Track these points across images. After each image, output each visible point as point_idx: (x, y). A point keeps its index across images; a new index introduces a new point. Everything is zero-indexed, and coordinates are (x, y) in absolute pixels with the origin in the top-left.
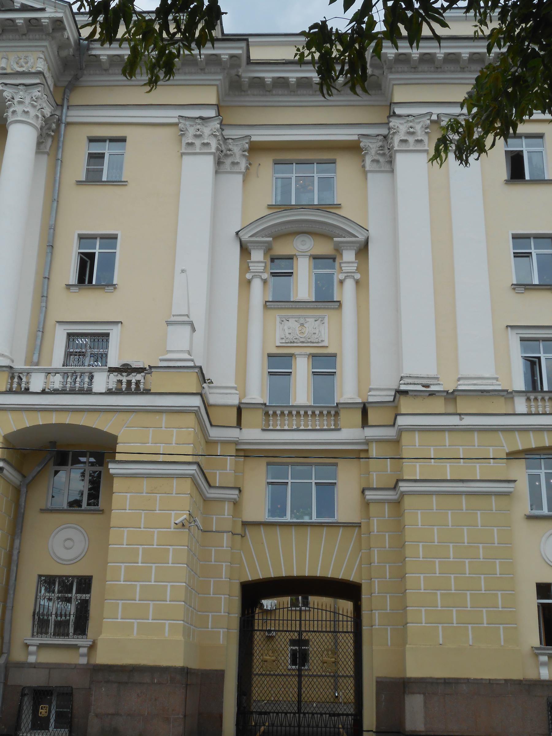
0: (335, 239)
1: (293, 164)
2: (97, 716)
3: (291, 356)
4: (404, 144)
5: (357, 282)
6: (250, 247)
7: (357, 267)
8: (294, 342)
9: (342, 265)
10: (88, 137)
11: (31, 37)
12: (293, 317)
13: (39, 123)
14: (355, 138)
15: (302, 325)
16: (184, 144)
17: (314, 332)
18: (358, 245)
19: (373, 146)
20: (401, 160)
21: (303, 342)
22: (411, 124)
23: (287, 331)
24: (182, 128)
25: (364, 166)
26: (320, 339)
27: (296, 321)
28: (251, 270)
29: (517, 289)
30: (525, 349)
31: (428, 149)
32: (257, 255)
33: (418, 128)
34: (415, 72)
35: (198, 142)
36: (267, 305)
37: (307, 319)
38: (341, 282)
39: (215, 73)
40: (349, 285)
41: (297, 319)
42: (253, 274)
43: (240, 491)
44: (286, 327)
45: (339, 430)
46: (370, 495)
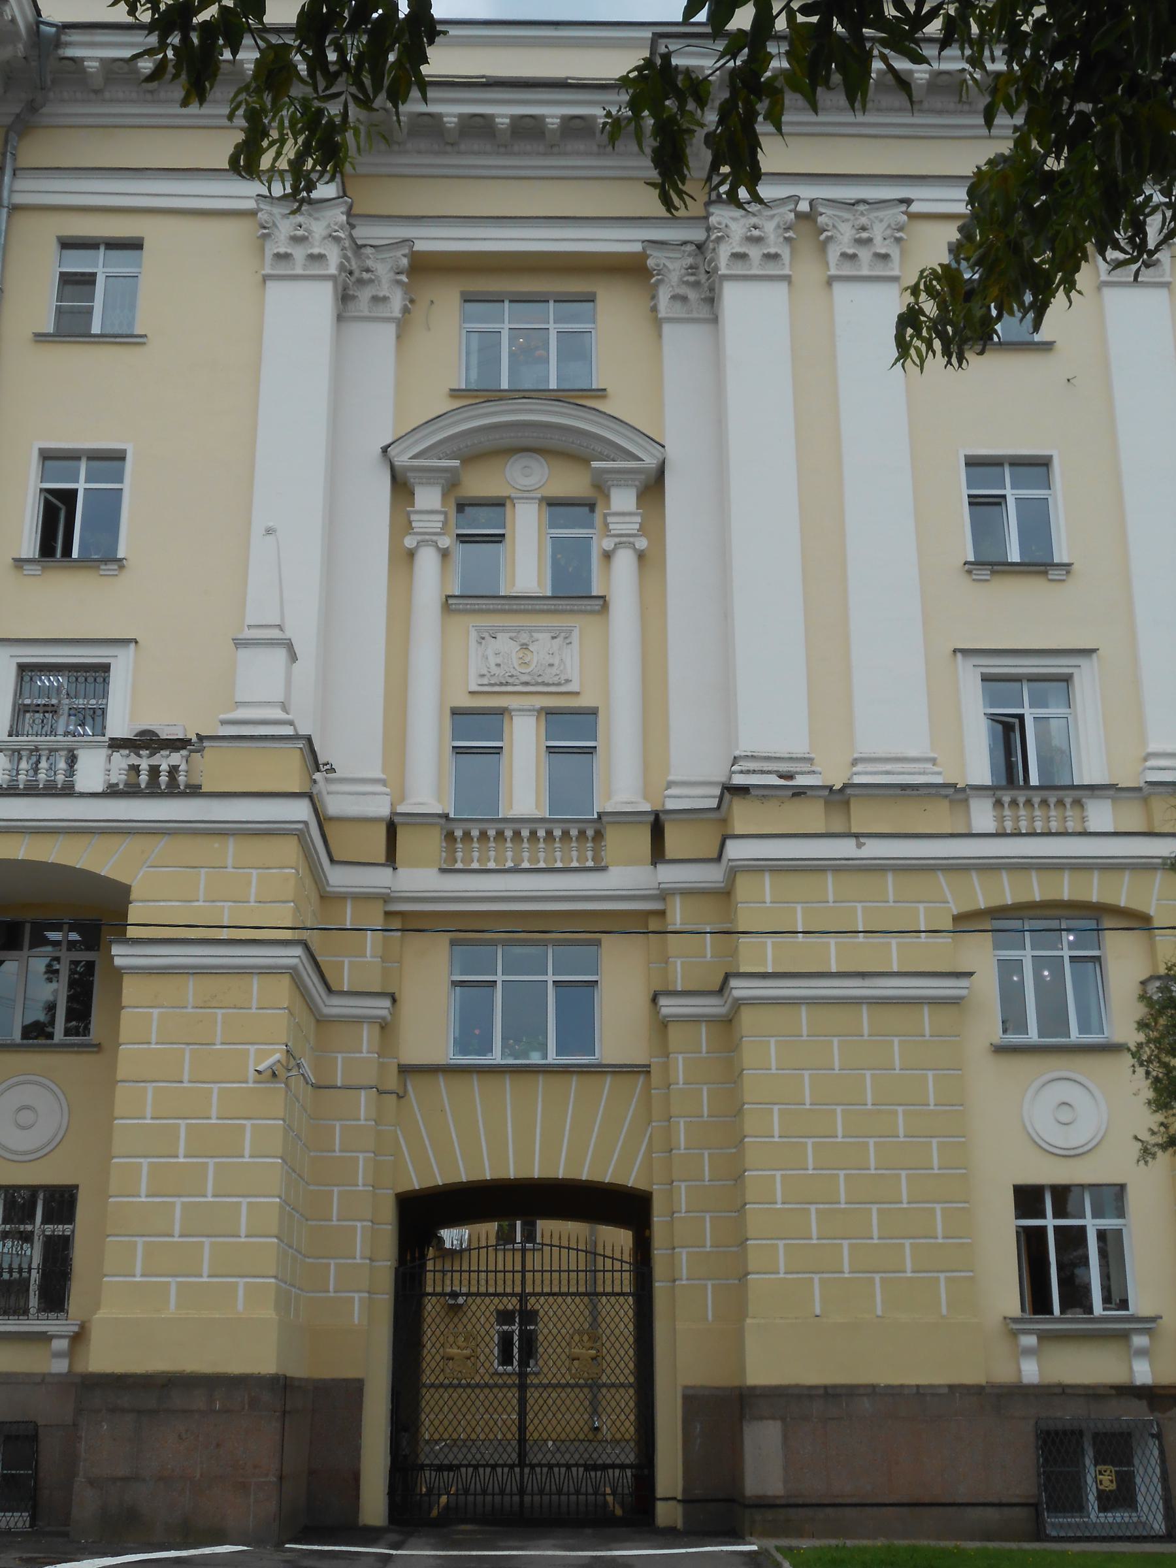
0: (595, 464)
1: (503, 301)
2: (92, 1482)
3: (502, 712)
5: (641, 556)
7: (641, 524)
8: (507, 684)
9: (610, 519)
12: (504, 630)
15: (525, 647)
16: (269, 254)
17: (551, 661)
18: (643, 477)
19: (674, 267)
20: (733, 296)
21: (526, 684)
23: (493, 661)
24: (266, 222)
25: (654, 309)
26: (563, 677)
27: (511, 638)
28: (415, 530)
29: (974, 572)
30: (991, 699)
31: (790, 273)
32: (428, 498)
35: (299, 253)
36: (449, 605)
38: (608, 556)
40: (624, 561)
41: (513, 635)
42: (419, 538)
43: (394, 1001)
45: (604, 869)
46: (669, 1006)
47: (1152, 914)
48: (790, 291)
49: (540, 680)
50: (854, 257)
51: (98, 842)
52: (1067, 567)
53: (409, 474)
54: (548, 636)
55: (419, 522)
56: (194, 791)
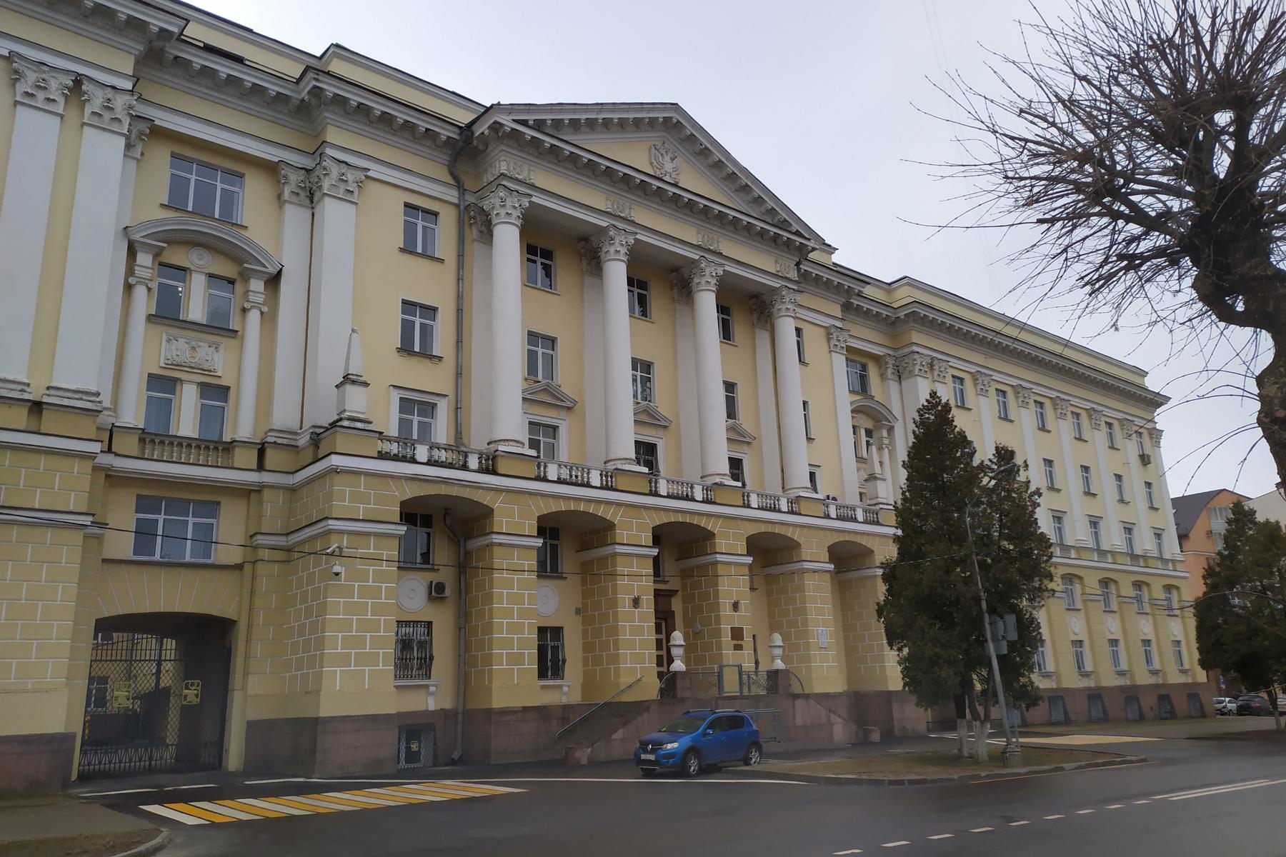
0: (245, 265)
3: (175, 380)
4: (349, 194)
6: (137, 248)
8: (182, 366)
10: (405, 202)
11: (741, 233)
13: (519, 223)
14: (881, 354)
15: (193, 348)
17: (207, 358)
18: (268, 276)
19: (294, 178)
22: (44, 76)
23: (174, 352)
25: (279, 196)
30: (531, 432)
31: (64, 114)
32: (144, 259)
33: (54, 84)
34: (394, 134)
36: (150, 318)
37: (200, 344)
39: (136, 41)
40: (254, 316)
41: (187, 341)
42: (138, 280)
44: (173, 347)
47: (875, 550)
48: (61, 124)
49: (201, 367)
50: (32, 95)
51: (1178, 580)
52: (440, 358)
53: (136, 244)
54: (207, 345)
55: (138, 271)
56: (714, 503)
